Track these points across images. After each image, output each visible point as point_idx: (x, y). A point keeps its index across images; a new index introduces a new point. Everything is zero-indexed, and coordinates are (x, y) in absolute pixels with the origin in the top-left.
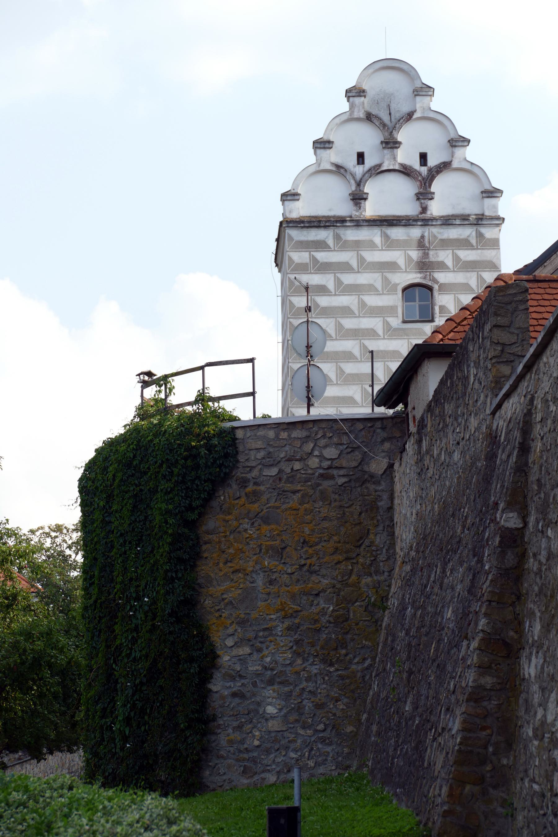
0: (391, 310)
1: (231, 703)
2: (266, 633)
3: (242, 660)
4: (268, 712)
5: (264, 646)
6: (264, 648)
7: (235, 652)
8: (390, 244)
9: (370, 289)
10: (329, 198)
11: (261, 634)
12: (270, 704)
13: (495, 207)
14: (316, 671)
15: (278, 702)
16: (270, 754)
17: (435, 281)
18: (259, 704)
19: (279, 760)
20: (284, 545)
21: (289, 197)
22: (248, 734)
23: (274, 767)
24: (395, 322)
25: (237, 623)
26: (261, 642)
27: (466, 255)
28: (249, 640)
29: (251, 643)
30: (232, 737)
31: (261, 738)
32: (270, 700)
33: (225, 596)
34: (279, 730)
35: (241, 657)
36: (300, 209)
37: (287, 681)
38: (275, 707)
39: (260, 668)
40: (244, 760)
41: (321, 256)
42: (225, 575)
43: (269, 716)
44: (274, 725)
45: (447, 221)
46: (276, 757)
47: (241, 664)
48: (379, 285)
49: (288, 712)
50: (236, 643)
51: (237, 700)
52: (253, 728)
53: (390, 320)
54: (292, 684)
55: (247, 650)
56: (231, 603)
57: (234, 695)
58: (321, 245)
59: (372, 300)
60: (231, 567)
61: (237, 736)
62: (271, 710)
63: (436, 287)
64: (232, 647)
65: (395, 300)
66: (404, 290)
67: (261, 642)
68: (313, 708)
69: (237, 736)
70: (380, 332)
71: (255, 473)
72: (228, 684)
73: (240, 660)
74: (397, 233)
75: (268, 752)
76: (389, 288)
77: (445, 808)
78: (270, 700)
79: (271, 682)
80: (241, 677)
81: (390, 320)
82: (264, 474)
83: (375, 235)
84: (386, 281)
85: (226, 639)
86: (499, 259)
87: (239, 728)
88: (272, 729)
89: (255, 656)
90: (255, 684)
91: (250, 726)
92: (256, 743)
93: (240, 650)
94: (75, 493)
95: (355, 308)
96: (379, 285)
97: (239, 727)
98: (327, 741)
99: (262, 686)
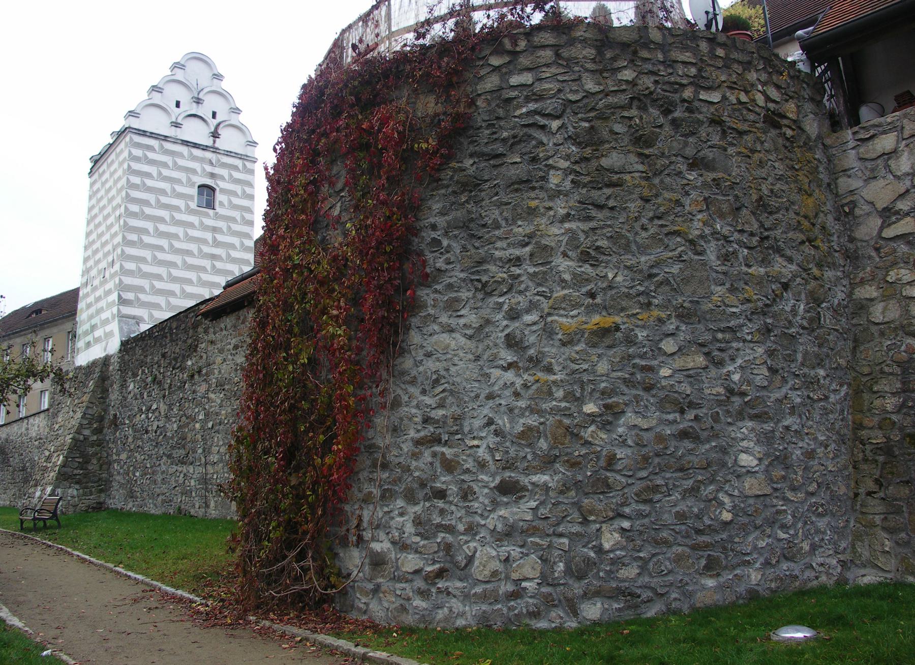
0: (191, 197)
1: (676, 448)
2: (728, 336)
3: (692, 376)
4: (743, 464)
5: (725, 355)
6: (727, 359)
7: (679, 363)
8: (194, 158)
9: (178, 181)
10: (156, 122)
11: (720, 336)
12: (746, 451)
13: (254, 152)
14: (799, 400)
15: (757, 449)
16: (748, 534)
17: (217, 185)
18: (724, 451)
19: (762, 544)
20: (738, 204)
21: (132, 114)
22: (710, 501)
23: (755, 556)
24: (193, 205)
25: (677, 316)
26: (721, 350)
27: (236, 175)
28: (702, 345)
29: (706, 350)
30: (681, 507)
31: (734, 507)
32: (745, 444)
33: (655, 271)
34: (760, 493)
35: (691, 372)
36: (135, 123)
37: (766, 413)
38: (753, 455)
39: (721, 390)
40: (707, 546)
41: (151, 155)
42: (653, 237)
43: (744, 470)
44: (752, 486)
45: (228, 153)
46: (757, 539)
47: (691, 383)
48: (184, 180)
49: (770, 464)
50: (680, 349)
51: (688, 444)
52: (718, 491)
53: (189, 203)
54: (772, 419)
55: (701, 360)
56: (667, 282)
57: (684, 435)
58: (150, 148)
59: (179, 189)
60: (662, 226)
61: (692, 505)
62: (746, 460)
63: (218, 189)
64: (674, 354)
65: (194, 191)
66: (199, 187)
67: (721, 350)
68: (802, 458)
69: (692, 505)
70: (183, 209)
71: (688, 93)
72: (670, 417)
73: (689, 376)
74: (197, 152)
75: (744, 529)
76: (191, 184)
77: (773, 585)
78: (745, 444)
79: (740, 415)
80: (691, 405)
81: (189, 203)
82: (701, 97)
83: (184, 150)
84: (189, 180)
85: (661, 340)
86: (253, 179)
87: (693, 491)
88: (749, 492)
89: (713, 372)
90: (716, 418)
91: (712, 487)
92: (727, 516)
93: (689, 359)
94: (293, 96)
95: (169, 191)
96: (184, 180)
97: (693, 488)
98: (820, 509)
99: (729, 420)
